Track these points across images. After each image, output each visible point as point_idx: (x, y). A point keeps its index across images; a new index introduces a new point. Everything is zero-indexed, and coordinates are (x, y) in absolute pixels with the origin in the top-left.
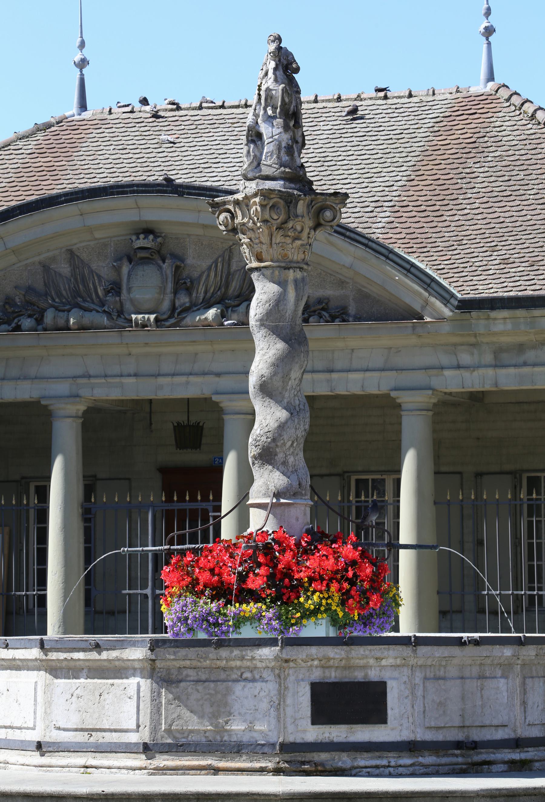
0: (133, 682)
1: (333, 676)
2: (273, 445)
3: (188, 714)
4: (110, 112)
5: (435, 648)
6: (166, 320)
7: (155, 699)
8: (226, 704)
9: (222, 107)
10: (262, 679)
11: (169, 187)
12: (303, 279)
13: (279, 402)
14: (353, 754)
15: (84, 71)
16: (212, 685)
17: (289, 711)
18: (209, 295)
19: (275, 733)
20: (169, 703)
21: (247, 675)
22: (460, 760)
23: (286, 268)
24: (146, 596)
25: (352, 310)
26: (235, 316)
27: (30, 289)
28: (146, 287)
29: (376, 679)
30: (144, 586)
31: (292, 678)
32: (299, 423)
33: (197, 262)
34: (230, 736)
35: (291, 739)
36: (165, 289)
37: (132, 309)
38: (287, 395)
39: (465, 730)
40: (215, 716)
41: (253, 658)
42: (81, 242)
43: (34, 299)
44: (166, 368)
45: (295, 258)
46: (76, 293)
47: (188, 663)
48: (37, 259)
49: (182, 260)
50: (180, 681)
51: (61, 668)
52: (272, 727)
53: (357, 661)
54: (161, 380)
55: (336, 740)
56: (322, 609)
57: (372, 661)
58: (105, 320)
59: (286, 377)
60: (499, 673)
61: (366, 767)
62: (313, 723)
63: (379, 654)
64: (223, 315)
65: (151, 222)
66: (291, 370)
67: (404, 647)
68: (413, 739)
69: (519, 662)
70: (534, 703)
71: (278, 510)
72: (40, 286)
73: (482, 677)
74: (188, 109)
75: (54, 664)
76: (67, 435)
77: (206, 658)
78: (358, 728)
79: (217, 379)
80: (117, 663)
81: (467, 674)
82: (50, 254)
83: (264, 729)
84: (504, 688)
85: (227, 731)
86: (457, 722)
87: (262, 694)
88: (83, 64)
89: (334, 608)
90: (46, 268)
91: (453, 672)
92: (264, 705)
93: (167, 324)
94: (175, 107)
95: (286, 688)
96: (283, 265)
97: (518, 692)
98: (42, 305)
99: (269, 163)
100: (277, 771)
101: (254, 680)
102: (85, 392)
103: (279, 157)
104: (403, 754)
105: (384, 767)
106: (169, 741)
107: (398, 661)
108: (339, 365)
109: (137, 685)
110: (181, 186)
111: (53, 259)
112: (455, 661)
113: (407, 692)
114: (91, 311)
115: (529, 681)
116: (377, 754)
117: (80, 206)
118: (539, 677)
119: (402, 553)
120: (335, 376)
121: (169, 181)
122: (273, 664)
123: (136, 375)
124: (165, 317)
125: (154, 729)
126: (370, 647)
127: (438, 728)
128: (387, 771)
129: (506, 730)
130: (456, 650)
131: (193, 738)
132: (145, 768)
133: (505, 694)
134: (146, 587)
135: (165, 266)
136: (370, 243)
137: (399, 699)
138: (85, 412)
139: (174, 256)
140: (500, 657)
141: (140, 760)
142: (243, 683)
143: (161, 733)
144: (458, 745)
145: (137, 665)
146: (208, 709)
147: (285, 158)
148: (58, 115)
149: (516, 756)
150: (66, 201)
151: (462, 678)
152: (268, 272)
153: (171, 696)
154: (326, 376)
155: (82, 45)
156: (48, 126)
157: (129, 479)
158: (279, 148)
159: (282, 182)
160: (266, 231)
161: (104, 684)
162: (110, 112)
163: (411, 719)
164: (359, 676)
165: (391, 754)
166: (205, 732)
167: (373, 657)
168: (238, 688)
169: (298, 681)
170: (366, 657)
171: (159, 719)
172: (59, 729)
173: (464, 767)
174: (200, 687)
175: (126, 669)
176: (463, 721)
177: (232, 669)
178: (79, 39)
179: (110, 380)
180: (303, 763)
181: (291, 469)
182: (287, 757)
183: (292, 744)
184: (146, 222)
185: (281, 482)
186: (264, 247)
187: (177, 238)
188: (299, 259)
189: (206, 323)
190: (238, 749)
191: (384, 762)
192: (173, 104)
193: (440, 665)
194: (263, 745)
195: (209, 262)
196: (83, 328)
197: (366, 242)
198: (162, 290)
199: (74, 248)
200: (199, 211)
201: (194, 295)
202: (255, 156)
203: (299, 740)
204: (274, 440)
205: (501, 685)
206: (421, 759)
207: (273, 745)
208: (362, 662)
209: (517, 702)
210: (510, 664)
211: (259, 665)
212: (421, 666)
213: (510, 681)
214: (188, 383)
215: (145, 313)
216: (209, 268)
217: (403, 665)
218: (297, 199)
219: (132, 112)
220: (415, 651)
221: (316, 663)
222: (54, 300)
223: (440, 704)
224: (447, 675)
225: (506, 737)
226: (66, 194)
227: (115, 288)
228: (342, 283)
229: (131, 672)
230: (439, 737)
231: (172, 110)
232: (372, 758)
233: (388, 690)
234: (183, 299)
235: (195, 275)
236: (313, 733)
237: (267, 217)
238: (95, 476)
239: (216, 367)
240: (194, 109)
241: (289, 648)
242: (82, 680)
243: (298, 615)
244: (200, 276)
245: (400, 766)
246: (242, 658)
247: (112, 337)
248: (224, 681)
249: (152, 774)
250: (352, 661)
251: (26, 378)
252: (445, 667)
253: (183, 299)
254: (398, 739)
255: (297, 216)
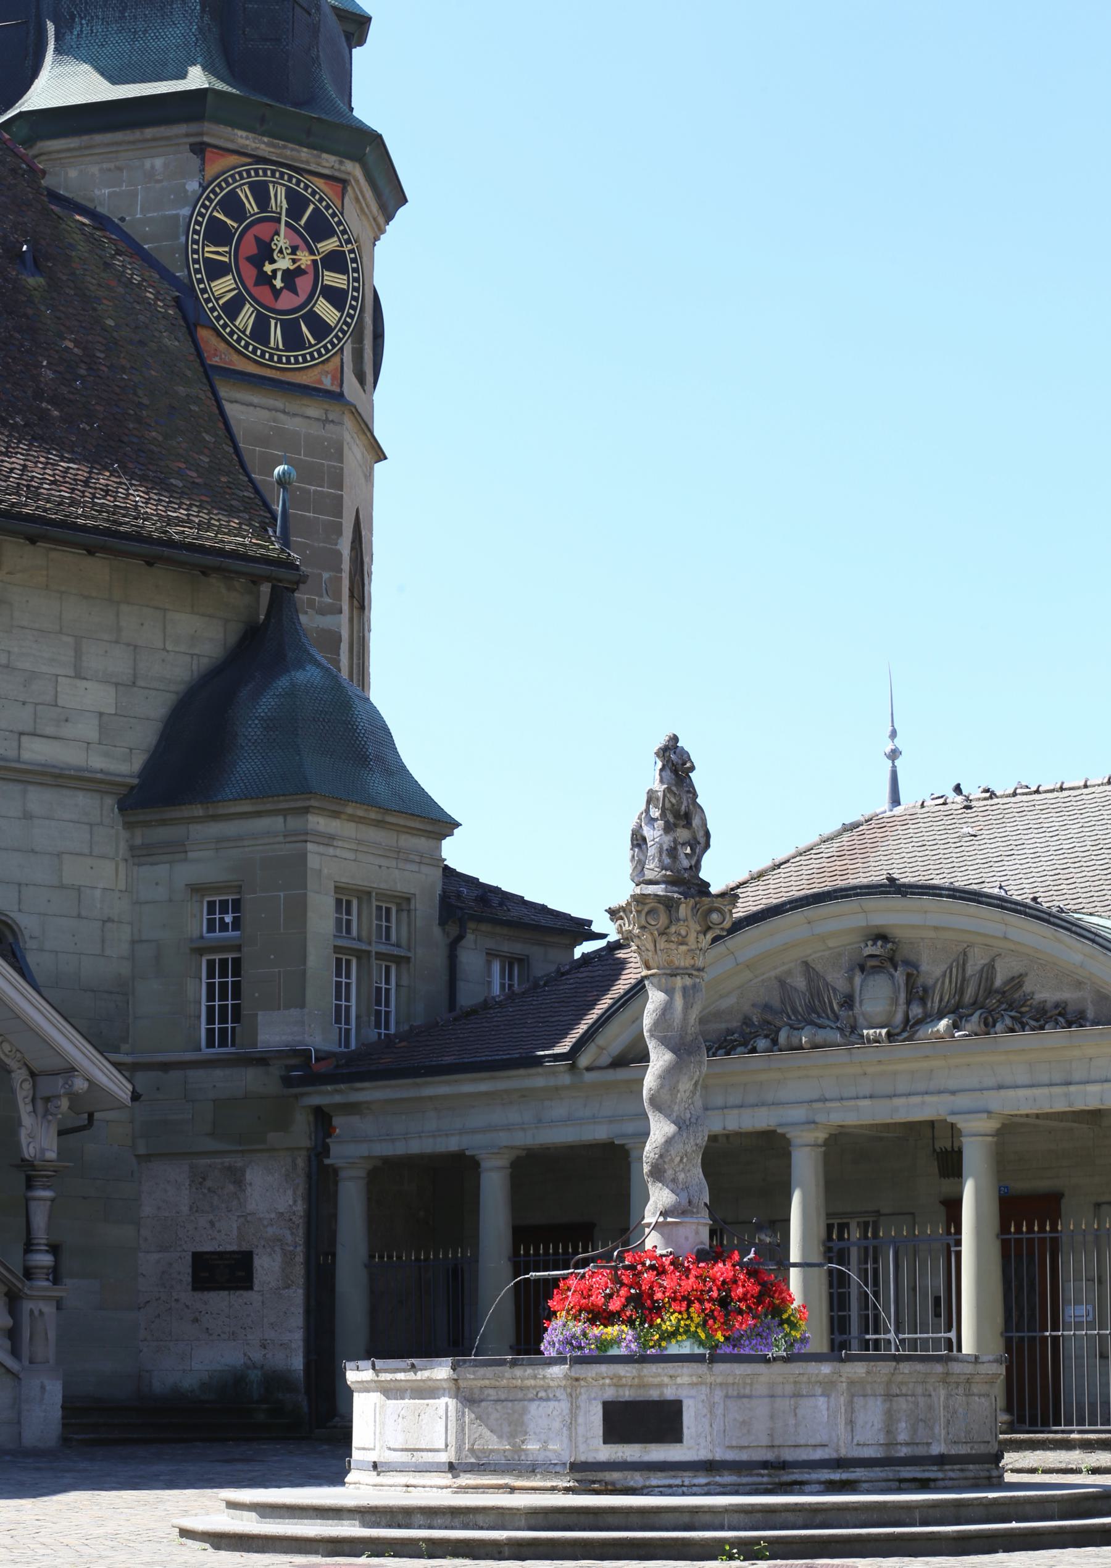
0: (444, 1400)
1: (627, 1395)
2: (661, 1161)
3: (489, 1433)
4: (922, 806)
5: (736, 1365)
6: (898, 1034)
7: (460, 1417)
8: (522, 1424)
9: (1037, 792)
10: (556, 1399)
11: (893, 887)
12: (694, 986)
13: (668, 1116)
14: (646, 1474)
15: (897, 762)
16: (510, 1404)
17: (581, 1430)
18: (944, 1004)
19: (568, 1452)
20: (472, 1423)
21: (542, 1394)
22: (765, 1479)
23: (672, 975)
24: (889, 1341)
25: (1090, 1014)
26: (969, 1026)
27: (767, 1007)
28: (878, 998)
29: (672, 1398)
30: (888, 1331)
31: (584, 1397)
32: (687, 1138)
33: (932, 969)
34: (527, 1455)
35: (582, 1458)
36: (897, 999)
37: (865, 1023)
38: (676, 1108)
39: (776, 1450)
40: (512, 1435)
41: (544, 1377)
42: (815, 952)
43: (769, 1018)
44: (902, 1088)
45: (682, 964)
46: (812, 1009)
47: (487, 1382)
48: (773, 974)
49: (916, 966)
50: (482, 1401)
51: (391, 1389)
52: (565, 1446)
53: (651, 1379)
54: (897, 1101)
55: (629, 1459)
56: (681, 1330)
57: (666, 1380)
58: (838, 1037)
59: (674, 1090)
60: (819, 1391)
61: (659, 1487)
62: (605, 1443)
63: (672, 1372)
64: (956, 1026)
65: (882, 926)
66: (678, 1082)
67: (699, 1365)
68: (710, 1457)
69: (843, 1379)
70: (866, 1423)
71: (666, 1230)
72: (776, 1003)
73: (797, 1395)
74: (1002, 797)
75: (385, 1385)
76: (805, 1167)
77: (503, 1377)
78: (653, 1447)
79: (952, 1098)
80: (430, 1383)
81: (779, 1391)
82: (785, 968)
83: (559, 1449)
84: (825, 1406)
85: (524, 1450)
86: (765, 1441)
87: (555, 1413)
88: (894, 754)
89: (693, 1329)
90: (782, 982)
91: (761, 1389)
92: (557, 1425)
93: (900, 1038)
94: (988, 795)
95: (578, 1407)
96: (668, 972)
97: (843, 1411)
98: (778, 1023)
99: (652, 866)
100: (567, 1490)
101: (548, 1399)
102: (821, 1118)
103: (660, 861)
104: (699, 1474)
105: (677, 1486)
106: (473, 1460)
107: (695, 1379)
108: (1077, 1077)
109: (446, 1404)
110: (904, 885)
111: (789, 973)
112: (762, 1379)
113: (705, 1411)
114: (825, 1027)
115: (859, 1402)
116: (672, 1473)
117: (805, 913)
118: (875, 1396)
119: (793, 1270)
120: (1072, 1088)
121: (891, 880)
122: (564, 1382)
123: (871, 1097)
124: (898, 1030)
125: (459, 1449)
126: (663, 1365)
127: (742, 1448)
128: (680, 1490)
129: (827, 1449)
130: (761, 1368)
131: (494, 1458)
132: (450, 1487)
133: (825, 1413)
134: (949, 1331)
135: (897, 974)
136: (1097, 939)
137: (696, 1418)
138: (826, 1143)
139: (907, 963)
140: (817, 1375)
141: (446, 1479)
142: (537, 1403)
143: (465, 1452)
144: (765, 1464)
145: (445, 1385)
146: (506, 1429)
147: (667, 861)
148: (868, 813)
149: (836, 1476)
150: (792, 909)
151: (772, 1396)
152: (655, 980)
153: (473, 1416)
154: (1064, 1089)
155: (893, 734)
156: (855, 826)
157: (913, 1214)
158: (661, 851)
159: (663, 886)
160: (650, 937)
161: (422, 1405)
162: (922, 806)
163: (709, 1438)
164: (654, 1395)
165: (685, 1474)
166: (505, 1451)
167: (666, 1375)
168: (533, 1407)
169: (590, 1400)
170: (659, 1375)
171: (464, 1439)
172: (390, 1449)
173: (770, 1487)
174: (499, 1407)
175: (438, 1389)
176: (772, 1441)
177: (528, 1388)
178: (890, 728)
179: (845, 1103)
180: (594, 1482)
181: (681, 1186)
182: (578, 1476)
183: (582, 1463)
184: (877, 926)
185: (669, 1200)
186: (650, 954)
187: (911, 943)
188: (687, 965)
189: (938, 1035)
190: (532, 1469)
191: (678, 1482)
192: (987, 791)
193: (745, 1383)
194: (555, 1464)
195: (943, 967)
196: (815, 1046)
197: (1092, 936)
198: (895, 1001)
199: (809, 959)
200: (926, 912)
201: (929, 1005)
202: (639, 861)
203: (590, 1460)
204: (661, 1156)
205: (820, 1403)
206: (718, 1479)
207: (565, 1464)
208: (656, 1380)
209: (842, 1421)
210: (832, 1382)
211: (552, 1384)
212: (721, 1384)
213: (832, 1399)
214: (923, 1103)
215: (873, 1028)
216: (944, 975)
217: (701, 1384)
218: (678, 903)
219: (945, 804)
220: (710, 1369)
221: (607, 1381)
222: (789, 1018)
223: (744, 1422)
224: (754, 1393)
225: (827, 1457)
226: (790, 902)
227: (848, 1002)
228: (1079, 984)
229: (441, 1392)
230: (744, 1456)
231: (985, 799)
232: (665, 1478)
233: (684, 1409)
234: (916, 1011)
235: (930, 982)
236: (606, 1453)
237: (643, 923)
238: (878, 1212)
239: (952, 1084)
240: (1008, 796)
241: (578, 1366)
242: (407, 1401)
243: (657, 1337)
244: (936, 983)
245: (694, 1485)
246: (535, 1377)
247: (838, 1056)
248: (521, 1400)
249: (456, 1493)
250: (646, 1380)
251: (763, 1104)
252: (751, 1384)
253: (916, 1011)
254: (696, 1458)
255: (678, 920)
